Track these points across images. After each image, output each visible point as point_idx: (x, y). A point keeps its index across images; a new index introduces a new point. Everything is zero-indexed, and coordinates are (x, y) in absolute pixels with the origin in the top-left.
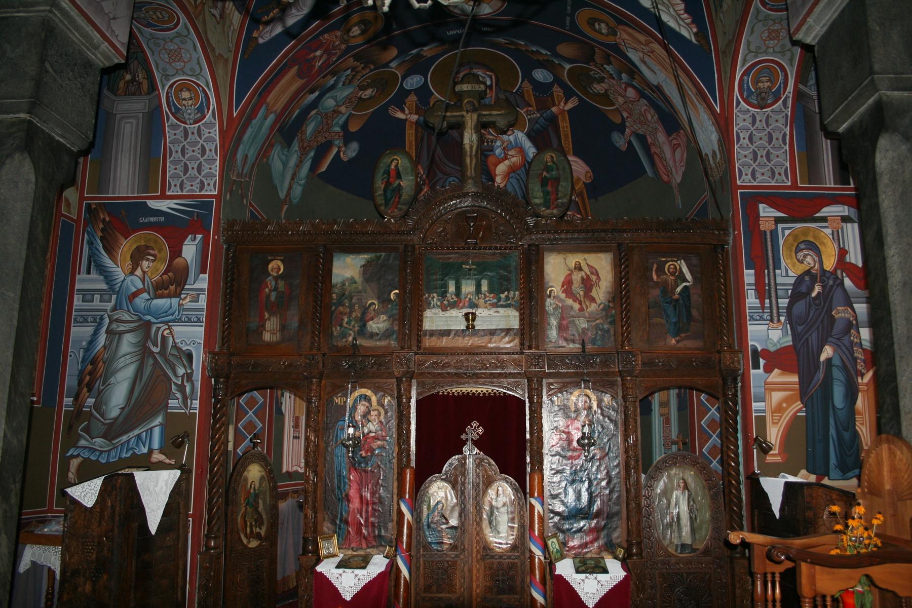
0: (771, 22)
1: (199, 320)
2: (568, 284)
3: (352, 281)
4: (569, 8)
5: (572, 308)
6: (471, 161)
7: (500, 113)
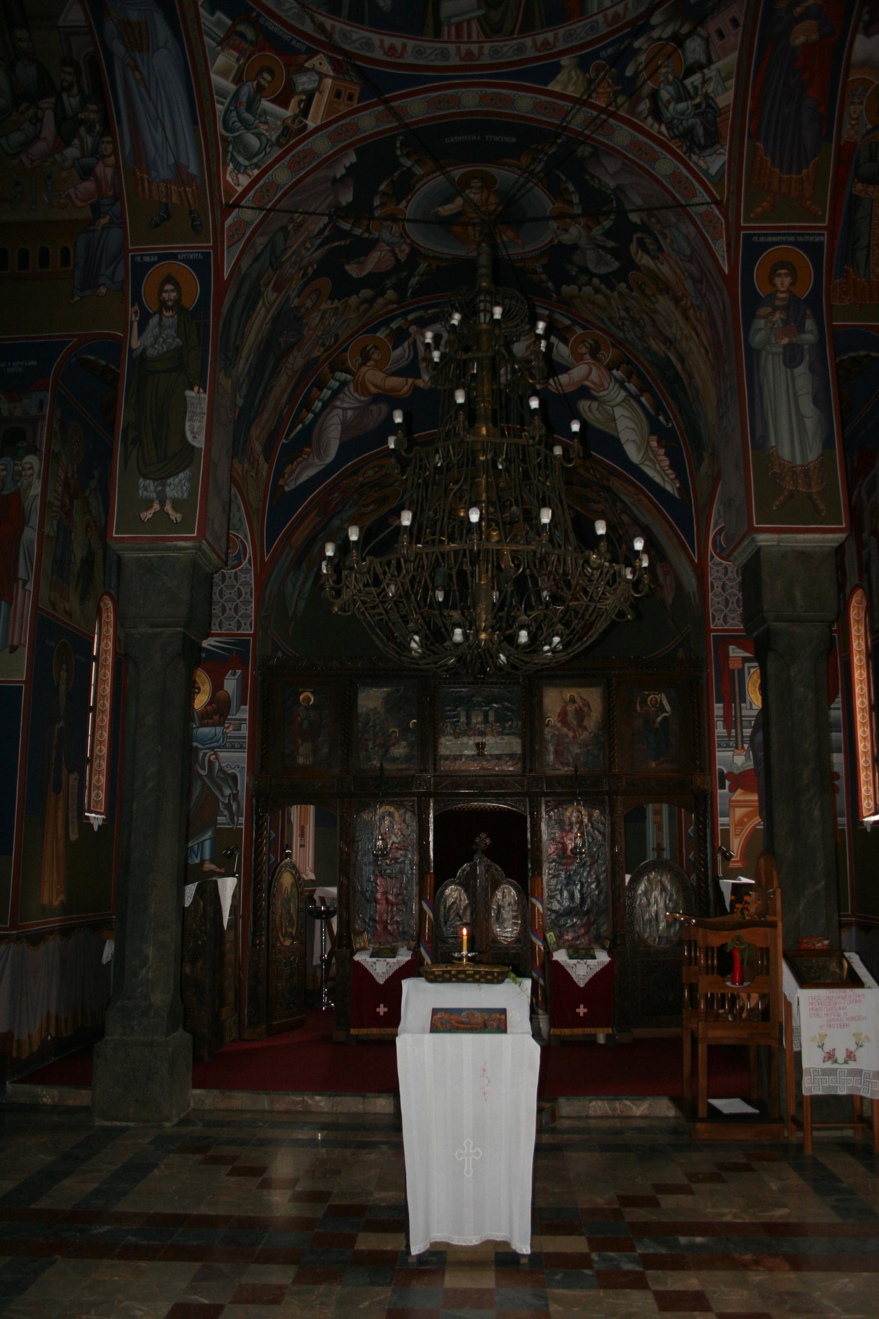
1: (242, 747)
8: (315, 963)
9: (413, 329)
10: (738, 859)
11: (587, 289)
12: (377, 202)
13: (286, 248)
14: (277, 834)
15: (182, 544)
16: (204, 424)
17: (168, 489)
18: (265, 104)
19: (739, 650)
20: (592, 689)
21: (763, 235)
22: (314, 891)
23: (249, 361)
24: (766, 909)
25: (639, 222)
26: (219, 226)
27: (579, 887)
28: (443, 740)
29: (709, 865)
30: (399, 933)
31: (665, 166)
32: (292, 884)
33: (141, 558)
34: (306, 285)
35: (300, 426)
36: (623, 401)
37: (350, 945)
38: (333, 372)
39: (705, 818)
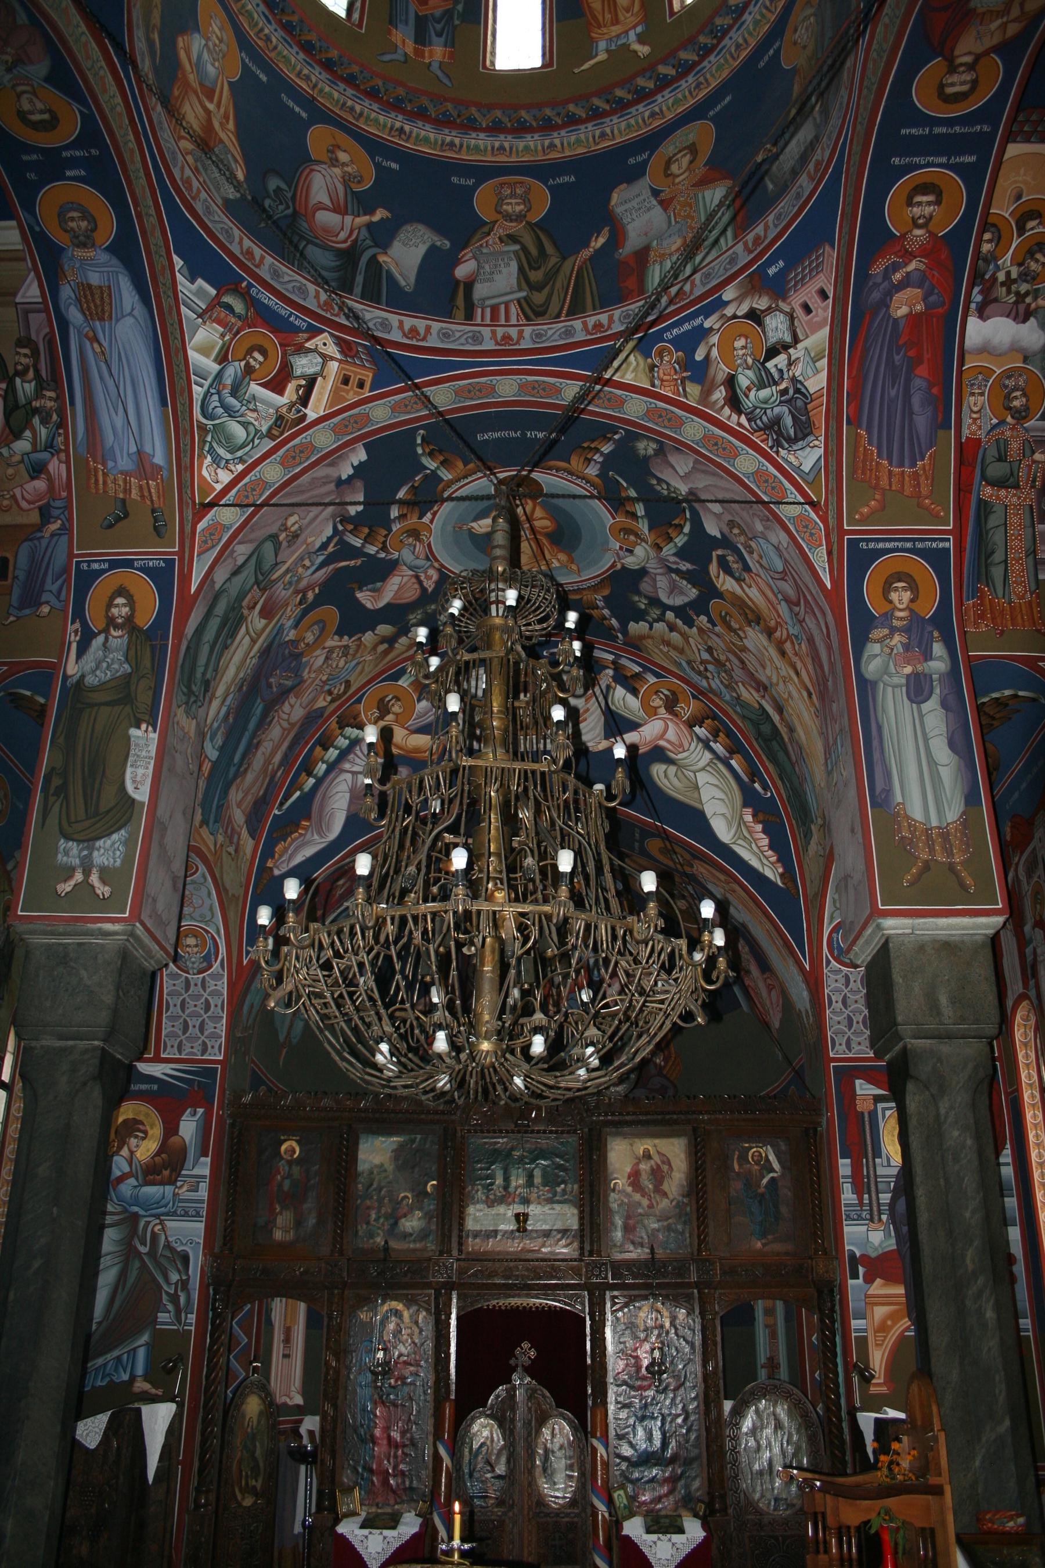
8: (296, 1531)
10: (881, 1381)
11: (659, 626)
12: (394, 512)
13: (277, 564)
14: (250, 1338)
15: (108, 927)
16: (150, 771)
17: (96, 854)
18: (255, 388)
20: (675, 1141)
21: (872, 540)
22: (301, 1421)
23: (227, 703)
24: (925, 1465)
25: (719, 536)
26: (188, 528)
27: (659, 1423)
28: (471, 1210)
29: (842, 1390)
30: (405, 1489)
31: (747, 463)
32: (261, 1413)
34: (305, 613)
35: (298, 793)
37: (333, 1508)
38: (342, 727)
39: (833, 1322)
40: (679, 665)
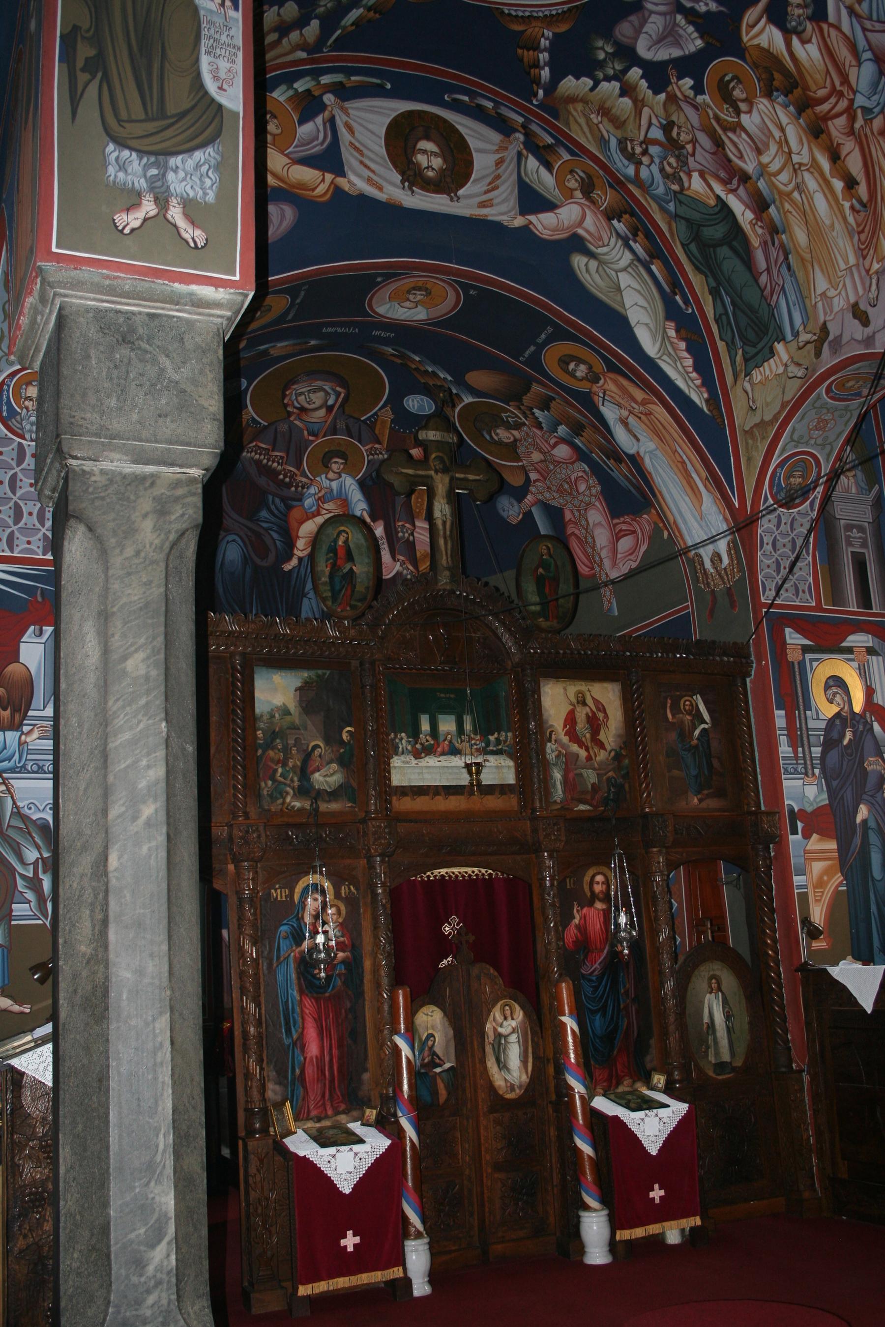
0: (825, 411)
1: (40, 770)
2: (571, 719)
3: (286, 712)
4: (543, 336)
5: (577, 755)
6: (446, 544)
7: (477, 478)
9: (328, 98)
15: (207, 292)
17: (171, 176)
19: (799, 636)
33: (107, 310)
36: (629, 265)
40: (603, 143)
